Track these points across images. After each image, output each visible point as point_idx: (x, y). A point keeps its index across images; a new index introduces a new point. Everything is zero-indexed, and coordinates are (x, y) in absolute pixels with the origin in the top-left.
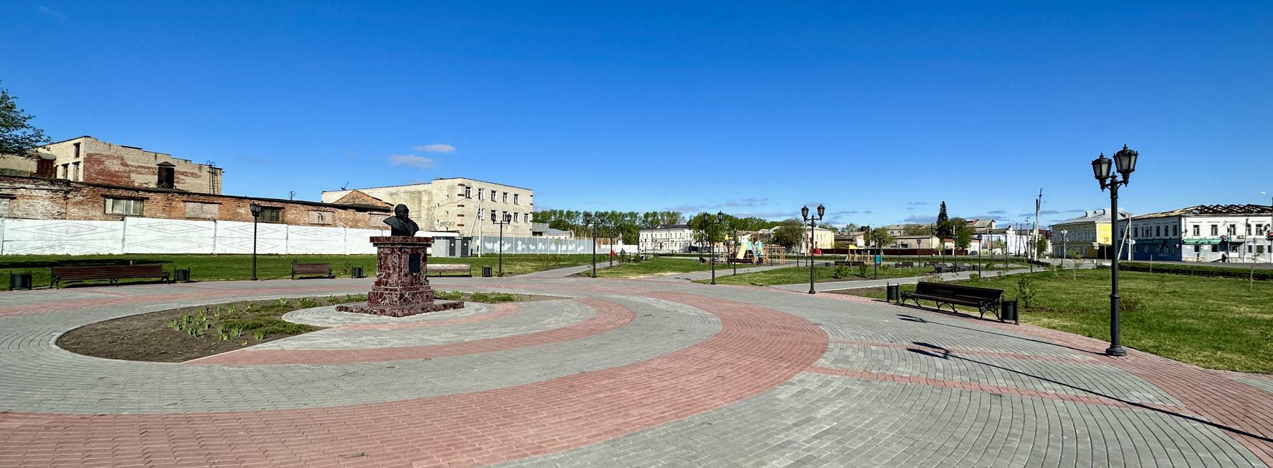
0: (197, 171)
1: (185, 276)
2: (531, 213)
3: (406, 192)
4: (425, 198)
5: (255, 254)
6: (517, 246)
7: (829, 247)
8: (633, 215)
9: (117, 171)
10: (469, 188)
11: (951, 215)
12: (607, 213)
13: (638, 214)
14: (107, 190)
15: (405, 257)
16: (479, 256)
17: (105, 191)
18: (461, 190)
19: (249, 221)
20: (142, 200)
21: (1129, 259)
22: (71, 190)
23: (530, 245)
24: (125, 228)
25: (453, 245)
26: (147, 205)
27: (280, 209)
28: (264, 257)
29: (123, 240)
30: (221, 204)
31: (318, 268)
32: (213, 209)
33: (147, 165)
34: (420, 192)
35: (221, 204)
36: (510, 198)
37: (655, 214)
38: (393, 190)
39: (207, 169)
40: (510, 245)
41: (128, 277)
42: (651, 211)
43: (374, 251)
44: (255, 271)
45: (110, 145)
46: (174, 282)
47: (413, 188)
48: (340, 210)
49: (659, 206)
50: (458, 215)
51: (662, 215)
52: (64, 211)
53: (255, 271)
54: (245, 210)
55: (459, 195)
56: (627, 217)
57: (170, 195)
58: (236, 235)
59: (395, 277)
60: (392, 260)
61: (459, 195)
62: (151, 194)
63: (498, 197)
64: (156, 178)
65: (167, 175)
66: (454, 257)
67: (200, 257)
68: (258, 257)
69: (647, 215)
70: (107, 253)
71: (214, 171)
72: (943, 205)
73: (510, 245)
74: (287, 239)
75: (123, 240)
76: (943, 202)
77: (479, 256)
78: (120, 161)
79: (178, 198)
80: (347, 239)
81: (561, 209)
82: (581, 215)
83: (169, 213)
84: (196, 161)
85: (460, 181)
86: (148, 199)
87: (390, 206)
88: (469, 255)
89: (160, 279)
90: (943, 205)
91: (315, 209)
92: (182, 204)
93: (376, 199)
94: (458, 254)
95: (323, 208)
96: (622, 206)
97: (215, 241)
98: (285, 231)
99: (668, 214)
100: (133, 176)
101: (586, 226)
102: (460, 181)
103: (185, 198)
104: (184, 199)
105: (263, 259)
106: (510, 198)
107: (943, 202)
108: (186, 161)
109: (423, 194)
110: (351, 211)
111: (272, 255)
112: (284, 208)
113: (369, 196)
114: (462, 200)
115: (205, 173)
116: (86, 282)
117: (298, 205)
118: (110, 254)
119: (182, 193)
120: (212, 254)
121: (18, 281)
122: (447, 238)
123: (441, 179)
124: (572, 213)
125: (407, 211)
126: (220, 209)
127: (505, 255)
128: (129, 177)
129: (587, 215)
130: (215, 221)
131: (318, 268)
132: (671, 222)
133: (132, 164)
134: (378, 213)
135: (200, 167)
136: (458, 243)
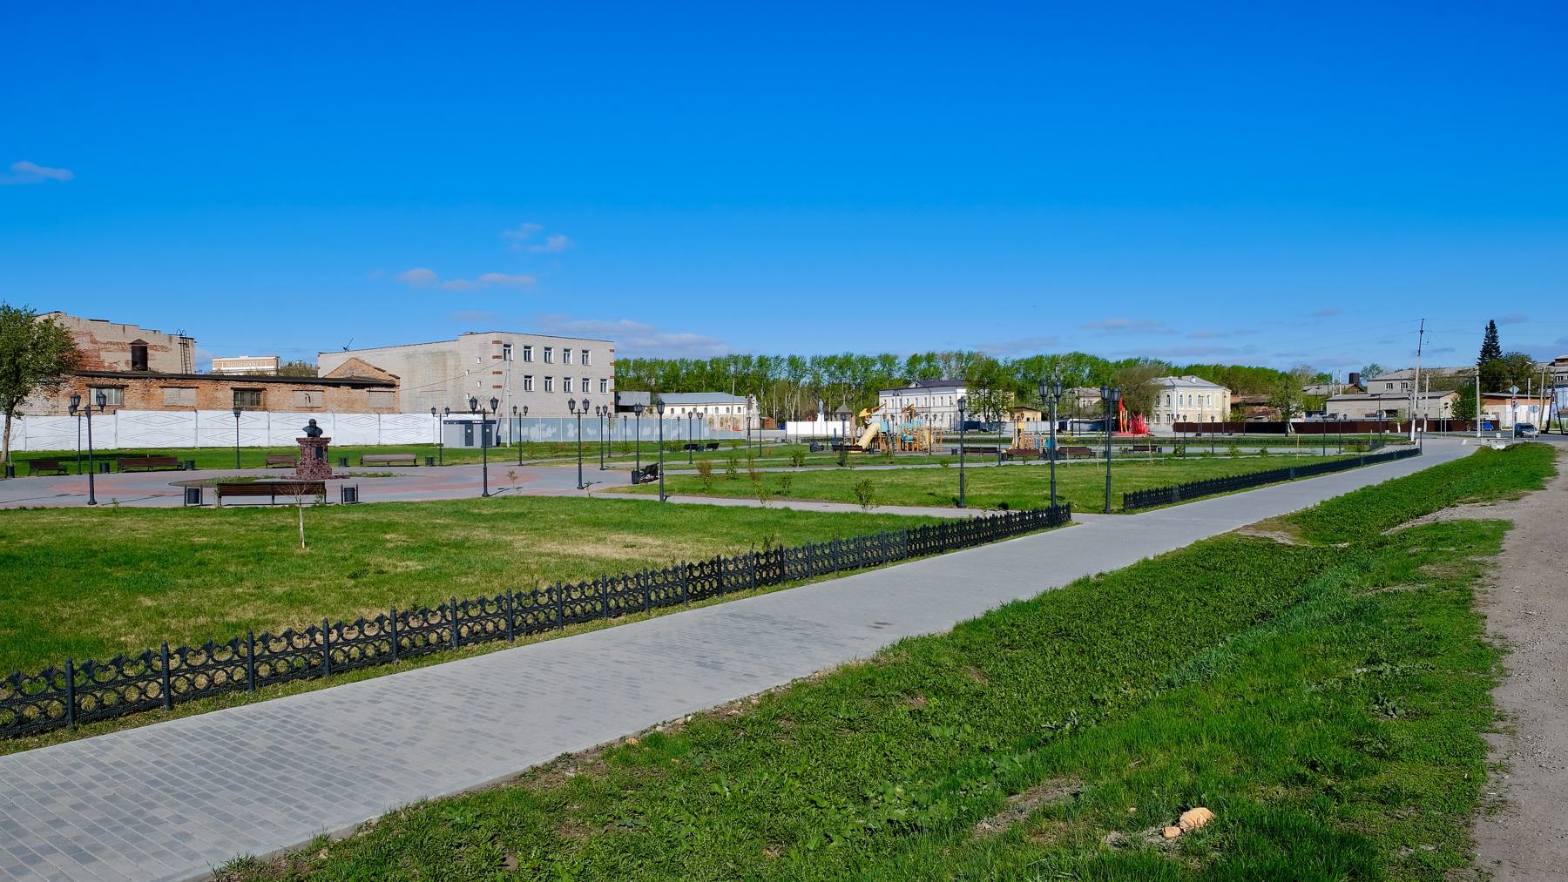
0: (166, 343)
1: (192, 465)
2: (611, 377)
3: (426, 354)
4: (451, 362)
5: (520, 443)
6: (566, 430)
7: (1218, 420)
8: (887, 360)
9: (87, 351)
10: (509, 346)
11: (1506, 345)
12: (834, 358)
13: (896, 358)
14: (90, 379)
15: (314, 449)
16: (508, 445)
17: (89, 380)
18: (497, 350)
19: (228, 409)
20: (122, 387)
21: (1399, 431)
22: (61, 382)
23: (588, 429)
24: (117, 422)
25: (469, 431)
26: (128, 393)
27: (260, 390)
28: (247, 450)
29: (116, 434)
30: (198, 388)
31: (287, 459)
32: (189, 395)
33: (116, 341)
34: (444, 354)
35: (198, 388)
36: (575, 357)
37: (930, 358)
38: (410, 350)
39: (177, 340)
40: (555, 430)
41: (158, 465)
42: (922, 351)
43: (297, 444)
44: (239, 463)
45: (79, 320)
46: (185, 470)
47: (435, 348)
48: (331, 388)
49: (904, 347)
50: (494, 387)
51: (947, 358)
52: (56, 404)
53: (239, 463)
54: (226, 393)
55: (494, 357)
56: (874, 365)
57: (147, 381)
58: (217, 425)
59: (309, 460)
60: (307, 451)
61: (494, 357)
62: (131, 381)
63: (555, 356)
64: (129, 356)
65: (140, 353)
66: (472, 447)
67: (184, 451)
68: (240, 450)
69: (914, 360)
70: (103, 448)
71: (185, 342)
72: (1492, 327)
73: (555, 430)
74: (269, 428)
75: (116, 434)
76: (1492, 323)
77: (508, 445)
78: (88, 337)
79: (156, 383)
80: (336, 427)
81: (746, 354)
82: (784, 365)
83: (147, 402)
84: (166, 331)
85: (494, 337)
86: (127, 386)
87: (394, 379)
88: (494, 443)
89: (176, 468)
90: (1492, 327)
91: (301, 388)
92: (160, 390)
93: (378, 369)
94: (478, 443)
95: (310, 387)
96: (864, 344)
97: (197, 433)
98: (267, 418)
99: (960, 356)
100: (104, 355)
101: (796, 383)
102: (494, 337)
103: (162, 383)
104: (162, 384)
105: (245, 453)
106: (575, 357)
107: (1492, 323)
108: (155, 331)
109: (448, 355)
110: (344, 389)
111: (254, 447)
112: (265, 389)
113: (369, 365)
114: (498, 365)
115: (176, 346)
116: (131, 469)
117: (282, 385)
118: (106, 449)
119: (159, 377)
120: (194, 448)
121: (104, 468)
122: (461, 422)
123: (472, 333)
124: (767, 360)
125: (315, 423)
126: (197, 394)
127: (643, 442)
128: (98, 357)
129: (793, 362)
130: (195, 411)
131: (287, 459)
132: (925, 375)
133: (101, 340)
134: (379, 389)
135: (170, 338)
136: (478, 430)
